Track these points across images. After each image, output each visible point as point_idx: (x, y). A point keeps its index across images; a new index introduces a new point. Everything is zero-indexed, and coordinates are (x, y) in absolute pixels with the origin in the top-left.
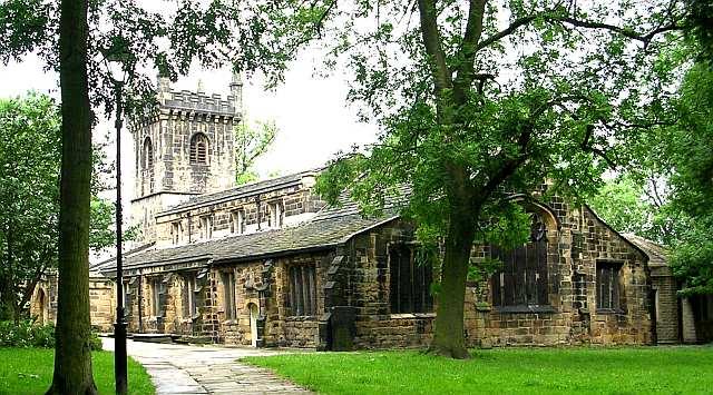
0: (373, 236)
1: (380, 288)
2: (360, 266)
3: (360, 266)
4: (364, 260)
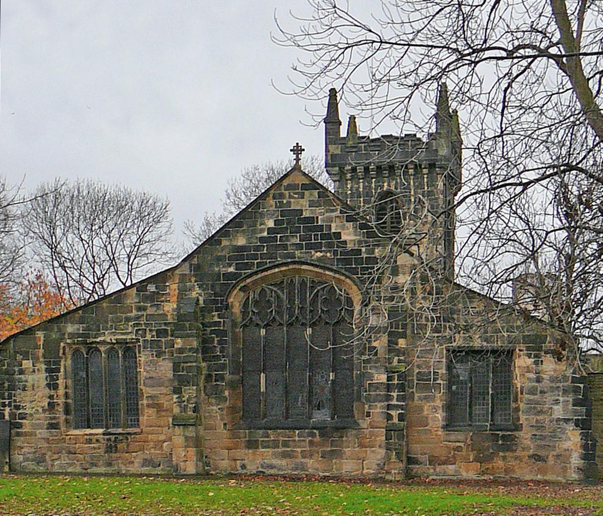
0: (40, 335)
1: (51, 397)
2: (21, 372)
3: (21, 372)
4: (27, 364)
